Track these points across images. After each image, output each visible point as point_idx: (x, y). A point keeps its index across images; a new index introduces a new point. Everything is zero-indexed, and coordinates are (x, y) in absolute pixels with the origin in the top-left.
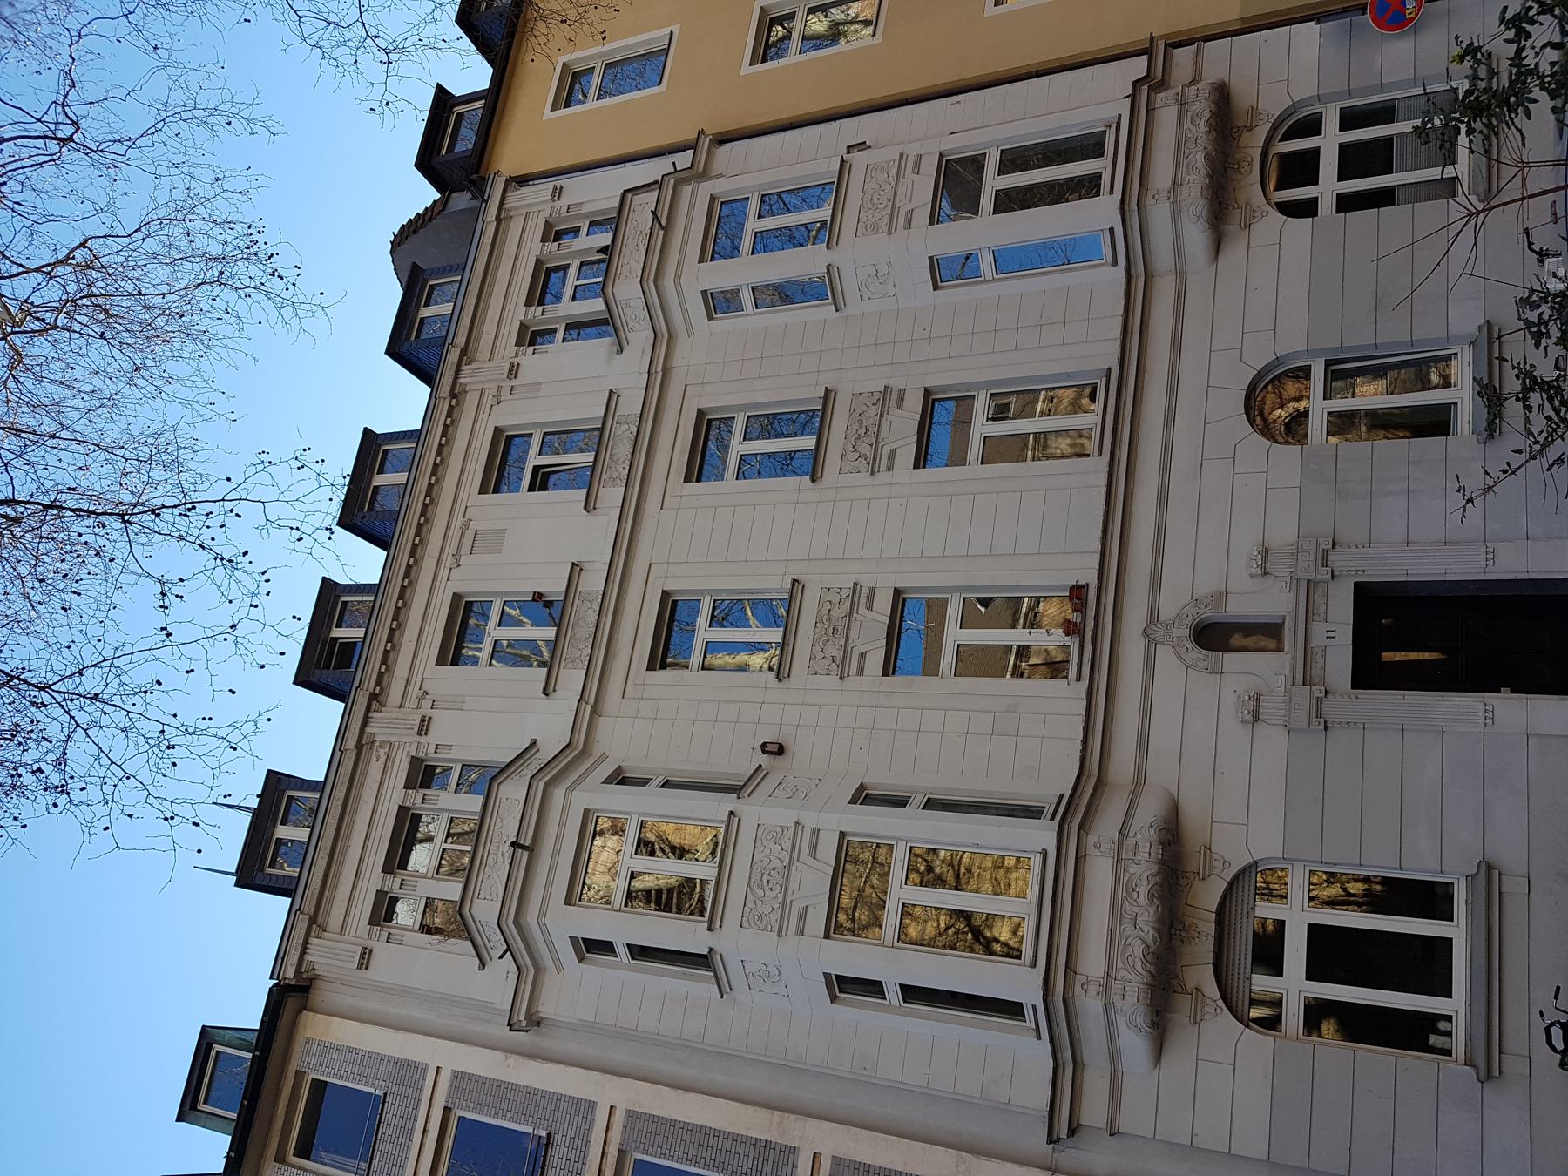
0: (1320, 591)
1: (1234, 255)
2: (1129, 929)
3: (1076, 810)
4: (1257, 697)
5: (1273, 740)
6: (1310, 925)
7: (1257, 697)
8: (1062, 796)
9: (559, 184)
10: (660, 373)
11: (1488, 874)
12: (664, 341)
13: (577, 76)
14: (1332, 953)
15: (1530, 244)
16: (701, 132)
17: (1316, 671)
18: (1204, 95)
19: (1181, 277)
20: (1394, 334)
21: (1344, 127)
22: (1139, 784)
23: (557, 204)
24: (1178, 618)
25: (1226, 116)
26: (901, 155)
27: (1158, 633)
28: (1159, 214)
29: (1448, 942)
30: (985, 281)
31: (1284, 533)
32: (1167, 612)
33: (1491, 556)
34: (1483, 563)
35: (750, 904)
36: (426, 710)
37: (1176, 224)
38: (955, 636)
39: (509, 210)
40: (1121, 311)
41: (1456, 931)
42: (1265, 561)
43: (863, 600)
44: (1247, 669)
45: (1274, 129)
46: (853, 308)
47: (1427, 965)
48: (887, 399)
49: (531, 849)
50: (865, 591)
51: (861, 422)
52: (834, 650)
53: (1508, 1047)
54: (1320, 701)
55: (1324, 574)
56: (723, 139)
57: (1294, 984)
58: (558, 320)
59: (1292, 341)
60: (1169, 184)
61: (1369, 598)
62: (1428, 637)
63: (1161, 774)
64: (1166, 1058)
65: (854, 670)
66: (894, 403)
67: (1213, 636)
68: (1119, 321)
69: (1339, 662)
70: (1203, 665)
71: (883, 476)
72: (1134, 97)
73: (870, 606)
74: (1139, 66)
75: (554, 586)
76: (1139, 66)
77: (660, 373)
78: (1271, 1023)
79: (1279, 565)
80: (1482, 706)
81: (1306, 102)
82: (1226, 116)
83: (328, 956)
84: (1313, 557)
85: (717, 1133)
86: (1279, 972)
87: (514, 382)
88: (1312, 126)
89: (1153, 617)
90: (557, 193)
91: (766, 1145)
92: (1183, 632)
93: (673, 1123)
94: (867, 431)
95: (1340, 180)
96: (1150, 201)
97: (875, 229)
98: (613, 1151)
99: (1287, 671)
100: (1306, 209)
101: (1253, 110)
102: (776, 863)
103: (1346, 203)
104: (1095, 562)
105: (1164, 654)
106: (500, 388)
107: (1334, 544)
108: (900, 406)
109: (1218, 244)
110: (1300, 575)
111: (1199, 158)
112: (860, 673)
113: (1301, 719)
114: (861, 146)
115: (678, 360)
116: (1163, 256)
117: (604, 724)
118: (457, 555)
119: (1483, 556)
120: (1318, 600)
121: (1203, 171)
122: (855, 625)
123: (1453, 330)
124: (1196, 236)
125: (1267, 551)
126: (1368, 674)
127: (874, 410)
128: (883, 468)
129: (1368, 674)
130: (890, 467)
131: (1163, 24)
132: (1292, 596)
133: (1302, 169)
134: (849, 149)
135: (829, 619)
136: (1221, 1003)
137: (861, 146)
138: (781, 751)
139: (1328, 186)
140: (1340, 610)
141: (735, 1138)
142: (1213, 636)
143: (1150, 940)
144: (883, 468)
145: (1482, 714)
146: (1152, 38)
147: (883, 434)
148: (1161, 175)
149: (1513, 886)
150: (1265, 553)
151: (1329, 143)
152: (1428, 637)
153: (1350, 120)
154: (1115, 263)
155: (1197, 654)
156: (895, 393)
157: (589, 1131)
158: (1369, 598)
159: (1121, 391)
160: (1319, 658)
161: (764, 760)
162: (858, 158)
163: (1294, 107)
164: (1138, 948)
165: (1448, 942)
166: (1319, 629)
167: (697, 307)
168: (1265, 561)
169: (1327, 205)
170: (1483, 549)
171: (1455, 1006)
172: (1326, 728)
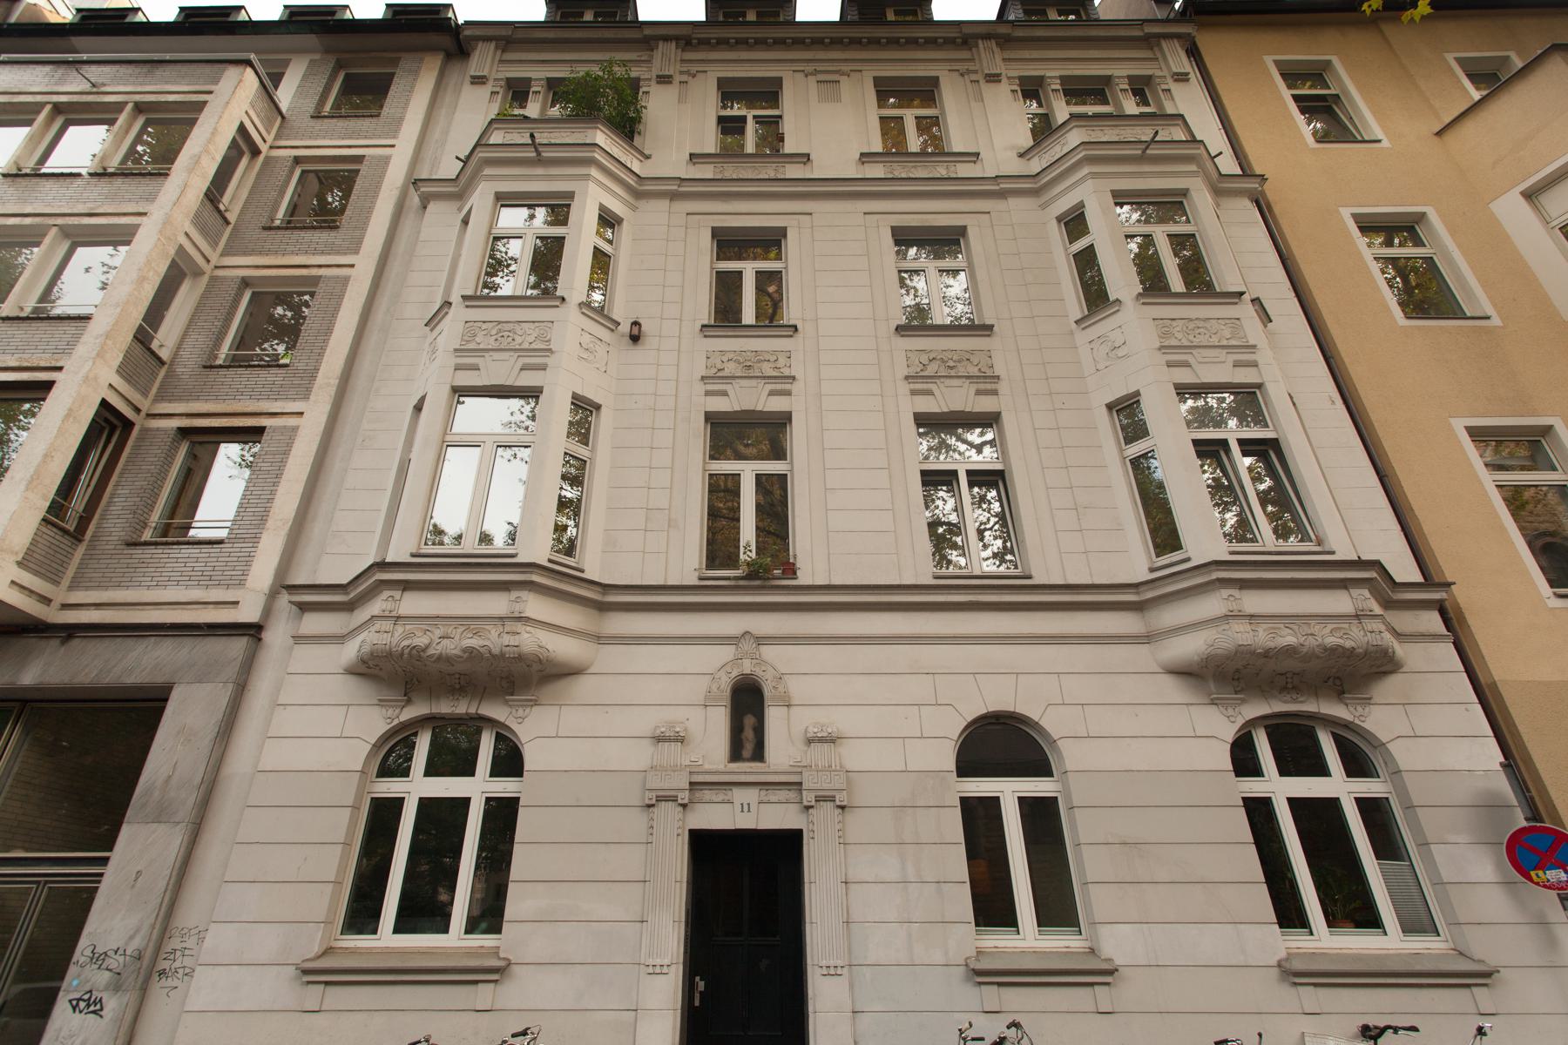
0: (792, 795)
1: (1172, 689)
2: (438, 633)
3: (561, 578)
4: (680, 739)
5: (640, 756)
6: (469, 799)
7: (680, 739)
8: (582, 571)
9: (1192, 76)
10: (999, 189)
11: (497, 972)
12: (1034, 187)
13: (1411, 230)
14: (442, 819)
15: (1396, 1030)
16: (1262, 178)
17: (707, 794)
18: (1374, 640)
19: (1147, 638)
20: (1089, 863)
21: (1364, 804)
22: (599, 639)
23: (1170, 80)
24: (760, 661)
25: (1355, 672)
26: (1254, 347)
27: (747, 646)
28: (1213, 605)
29: (446, 930)
30: (1121, 451)
31: (855, 757)
32: (768, 652)
33: (831, 972)
34: (824, 963)
35: (484, 326)
36: (677, 78)
37: (1202, 626)
38: (748, 472)
39: (1159, 45)
40: (1097, 581)
41: (456, 939)
42: (822, 740)
43: (779, 387)
44: (711, 734)
45: (1347, 725)
46: (1082, 337)
47: (423, 911)
48: (987, 381)
49: (539, 161)
50: (787, 387)
51: (959, 361)
52: (730, 369)
53: (331, 990)
54: (674, 799)
55: (808, 798)
56: (1263, 207)
57: (417, 787)
58: (1050, 106)
59: (1071, 755)
60: (1250, 610)
61: (787, 845)
62: (746, 902)
63: (610, 657)
64: (349, 677)
65: (710, 387)
66: (982, 386)
67: (747, 701)
68: (1088, 581)
69: (718, 816)
70: (714, 688)
71: (904, 388)
72: (1360, 564)
73: (772, 393)
74: (1404, 569)
75: (789, 147)
76: (1404, 569)
77: (999, 189)
78: (385, 771)
79: (819, 754)
80: (666, 962)
81: (1389, 758)
82: (1355, 672)
83: (483, 60)
84: (825, 786)
85: (326, 341)
86: (428, 773)
87: (982, 82)
88: (1357, 765)
89: (761, 640)
90: (1182, 78)
91: (313, 377)
92: (747, 667)
93: (337, 310)
94: (951, 368)
95: (1289, 799)
96: (1225, 593)
97: (1165, 335)
98: (314, 272)
99: (707, 767)
100: (1244, 761)
101: (1368, 701)
102: (519, 339)
103: (1259, 812)
104: (820, 580)
105: (726, 653)
106: (976, 72)
107: (843, 808)
108: (979, 393)
109: (1188, 673)
110: (805, 774)
111: (1288, 639)
112: (708, 393)
113: (656, 782)
114: (1266, 318)
115: (1013, 202)
116: (1170, 616)
117: (664, 204)
118: (816, 72)
119: (832, 963)
120: (783, 794)
121: (1272, 645)
122: (753, 382)
123: (1104, 931)
124: (1190, 647)
125: (833, 741)
126: (705, 845)
127: (974, 371)
128: (912, 386)
129: (705, 845)
130: (914, 393)
131: (1464, 595)
132: (785, 768)
133: (1298, 754)
134: (1256, 301)
135: (760, 361)
136: (396, 722)
137: (1266, 318)
138: (635, 339)
139: (1280, 788)
140: (774, 816)
141: (321, 355)
142: (747, 701)
143: (431, 651)
144: (912, 386)
145: (658, 962)
146: (1449, 585)
147: (948, 382)
148: (1256, 602)
149: (483, 995)
150: (831, 740)
151: (1336, 785)
152: (746, 902)
153: (1372, 810)
154: (1152, 570)
155: (725, 683)
156: (993, 386)
157: (338, 253)
158: (787, 845)
159: (1016, 593)
160: (721, 797)
161: (625, 328)
162: (1246, 311)
163: (1380, 745)
164: (421, 641)
165: (446, 930)
166: (751, 795)
167: (1064, 204)
168: (822, 740)
169: (1253, 787)
170: (839, 963)
171: (386, 938)
172: (650, 806)
